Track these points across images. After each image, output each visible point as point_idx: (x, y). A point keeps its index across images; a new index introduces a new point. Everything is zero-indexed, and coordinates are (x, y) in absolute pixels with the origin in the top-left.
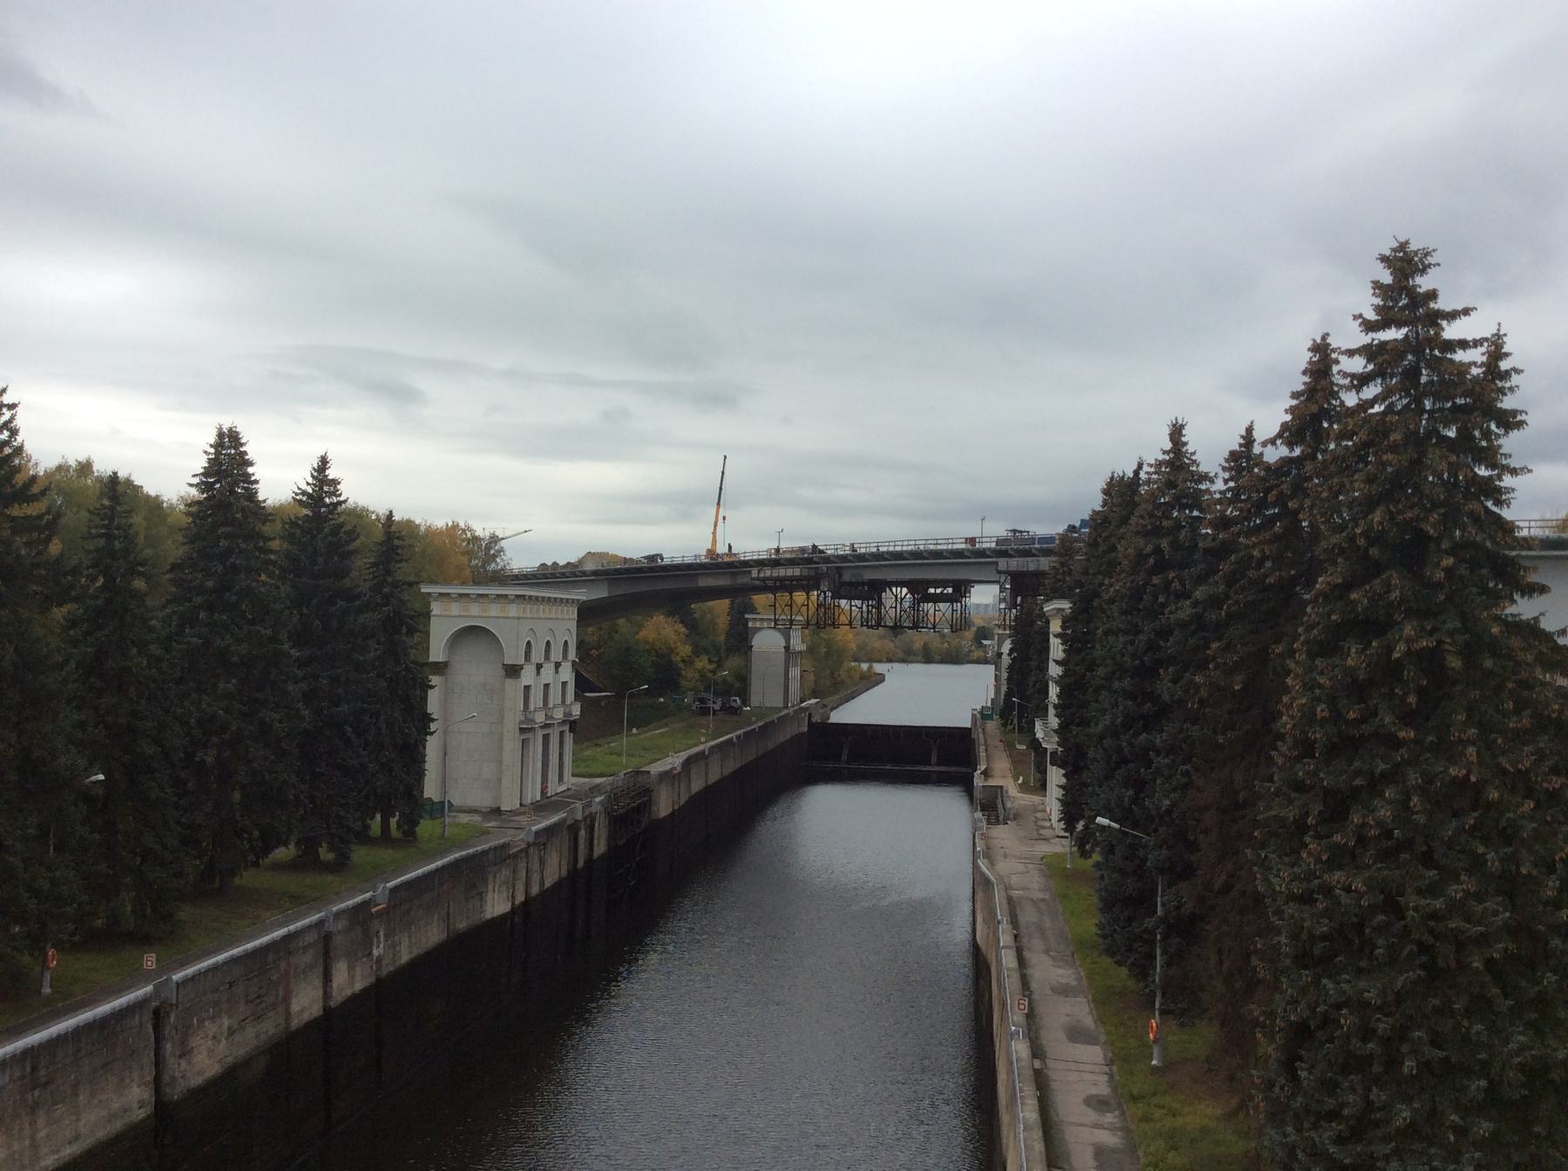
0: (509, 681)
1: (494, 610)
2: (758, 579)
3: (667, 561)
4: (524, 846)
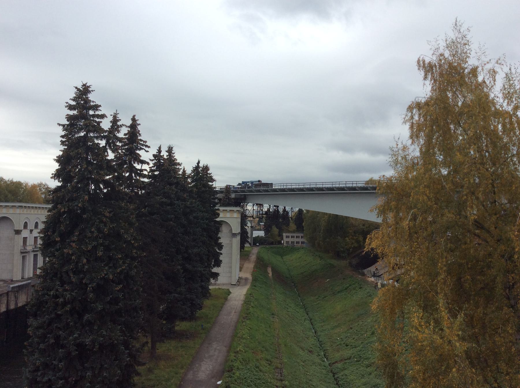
0: (16, 235)
1: (11, 211)
4: (6, 291)
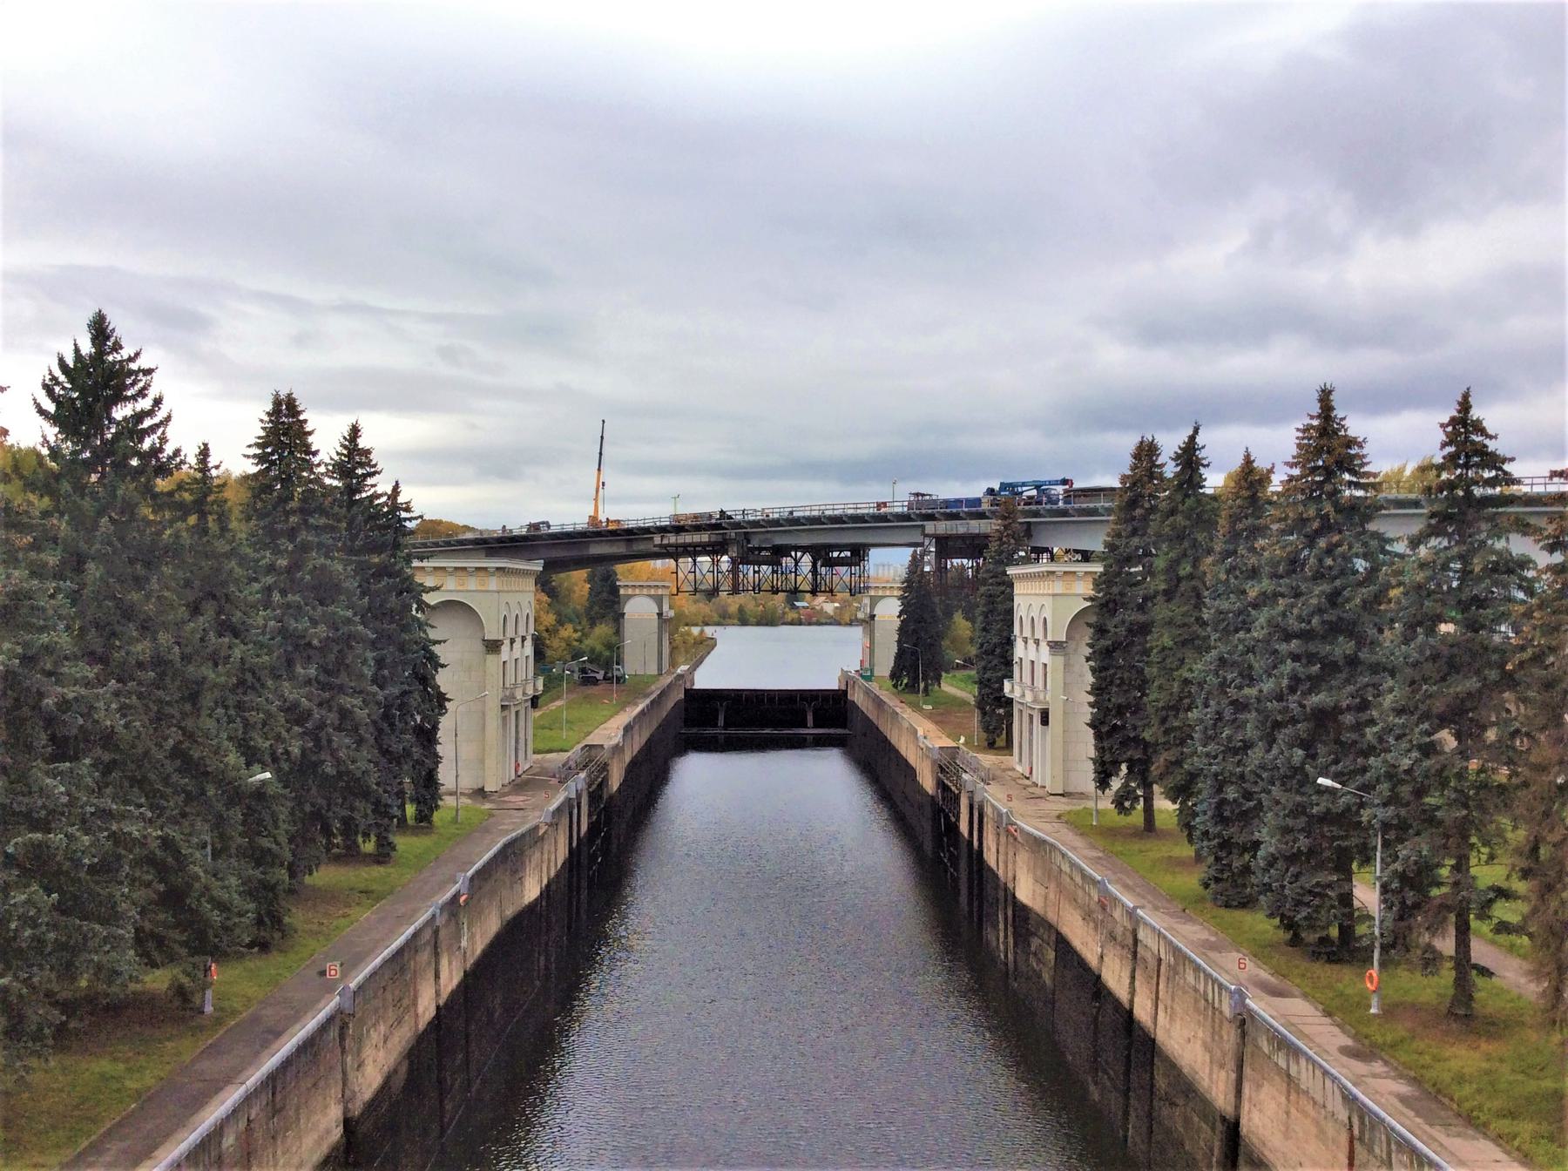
0: (490, 658)
1: (472, 583)
2: (661, 546)
3: (553, 530)
